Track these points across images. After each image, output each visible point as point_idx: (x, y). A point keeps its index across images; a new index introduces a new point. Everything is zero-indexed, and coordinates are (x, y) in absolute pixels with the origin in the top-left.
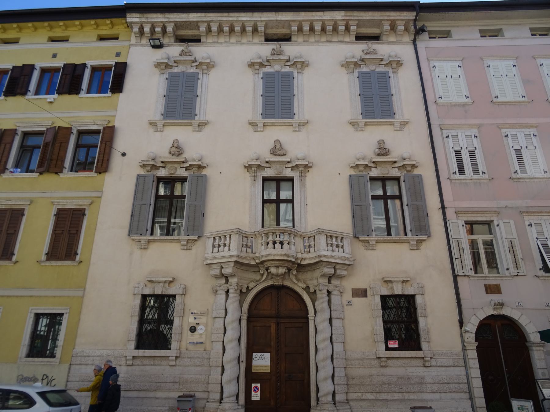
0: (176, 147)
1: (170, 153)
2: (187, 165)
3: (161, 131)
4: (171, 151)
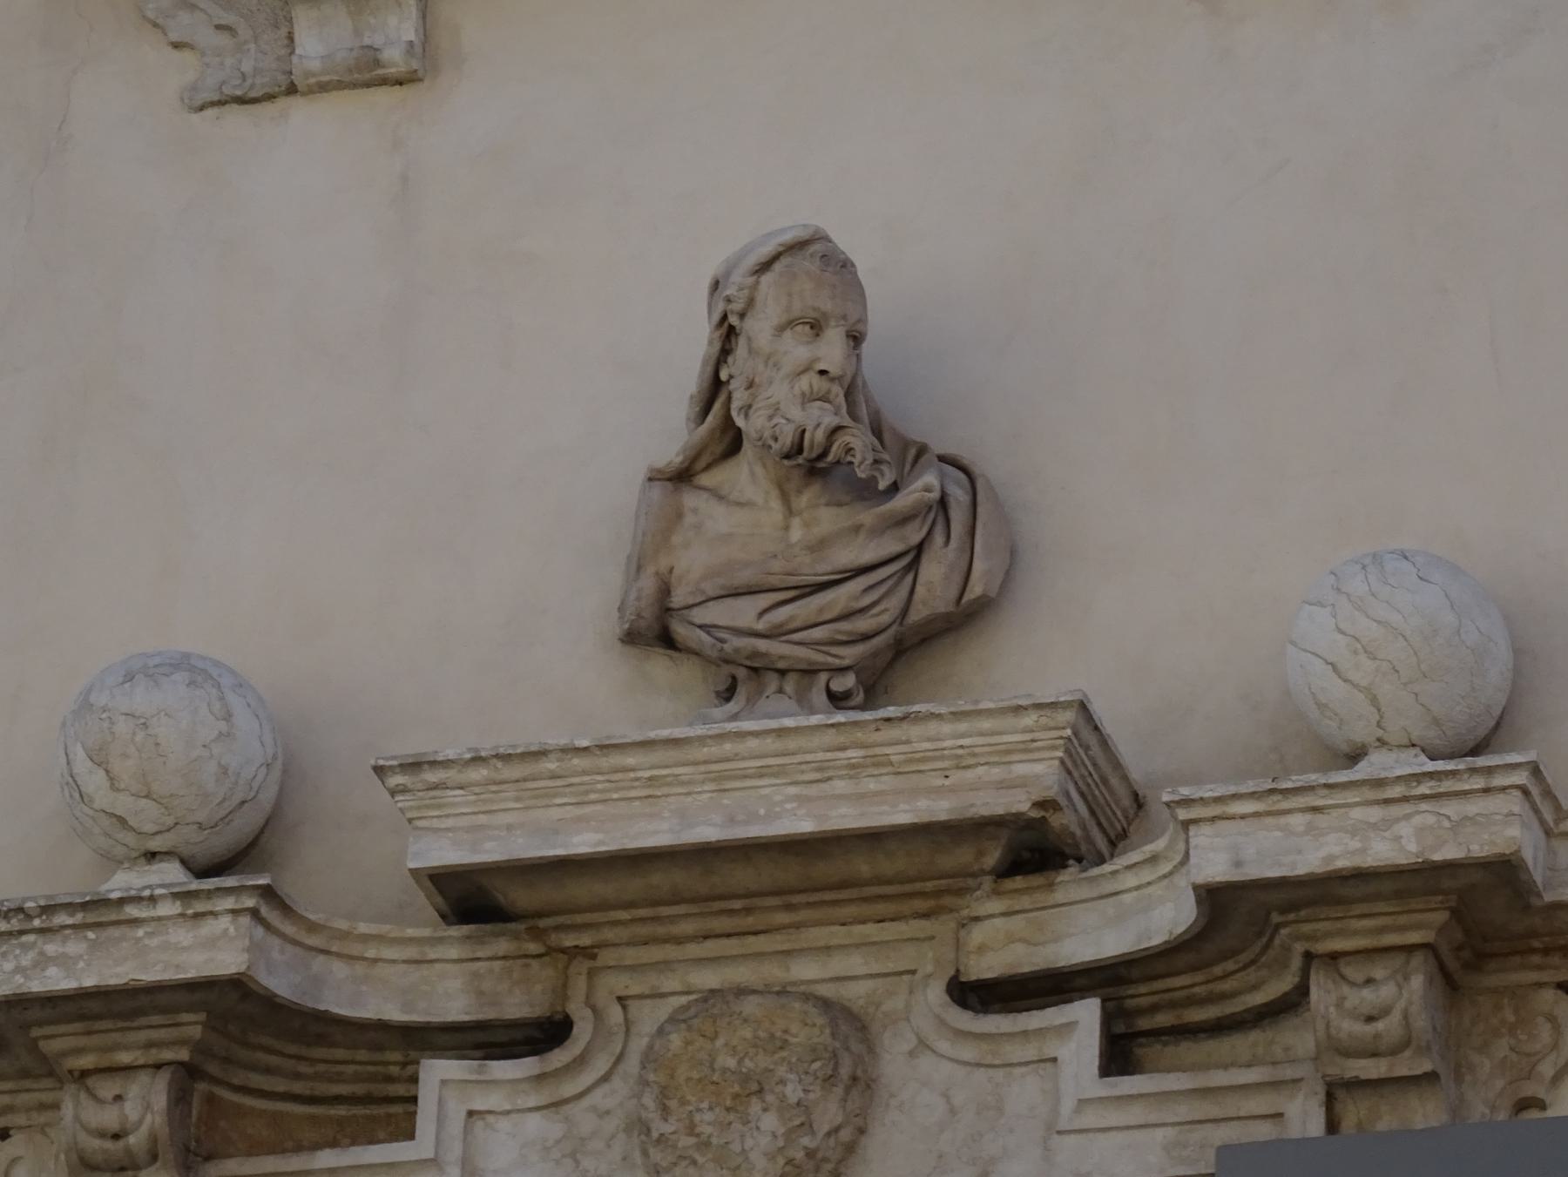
0: (810, 465)
1: (655, 632)
2: (1126, 911)
3: (367, 74)
4: (692, 562)
